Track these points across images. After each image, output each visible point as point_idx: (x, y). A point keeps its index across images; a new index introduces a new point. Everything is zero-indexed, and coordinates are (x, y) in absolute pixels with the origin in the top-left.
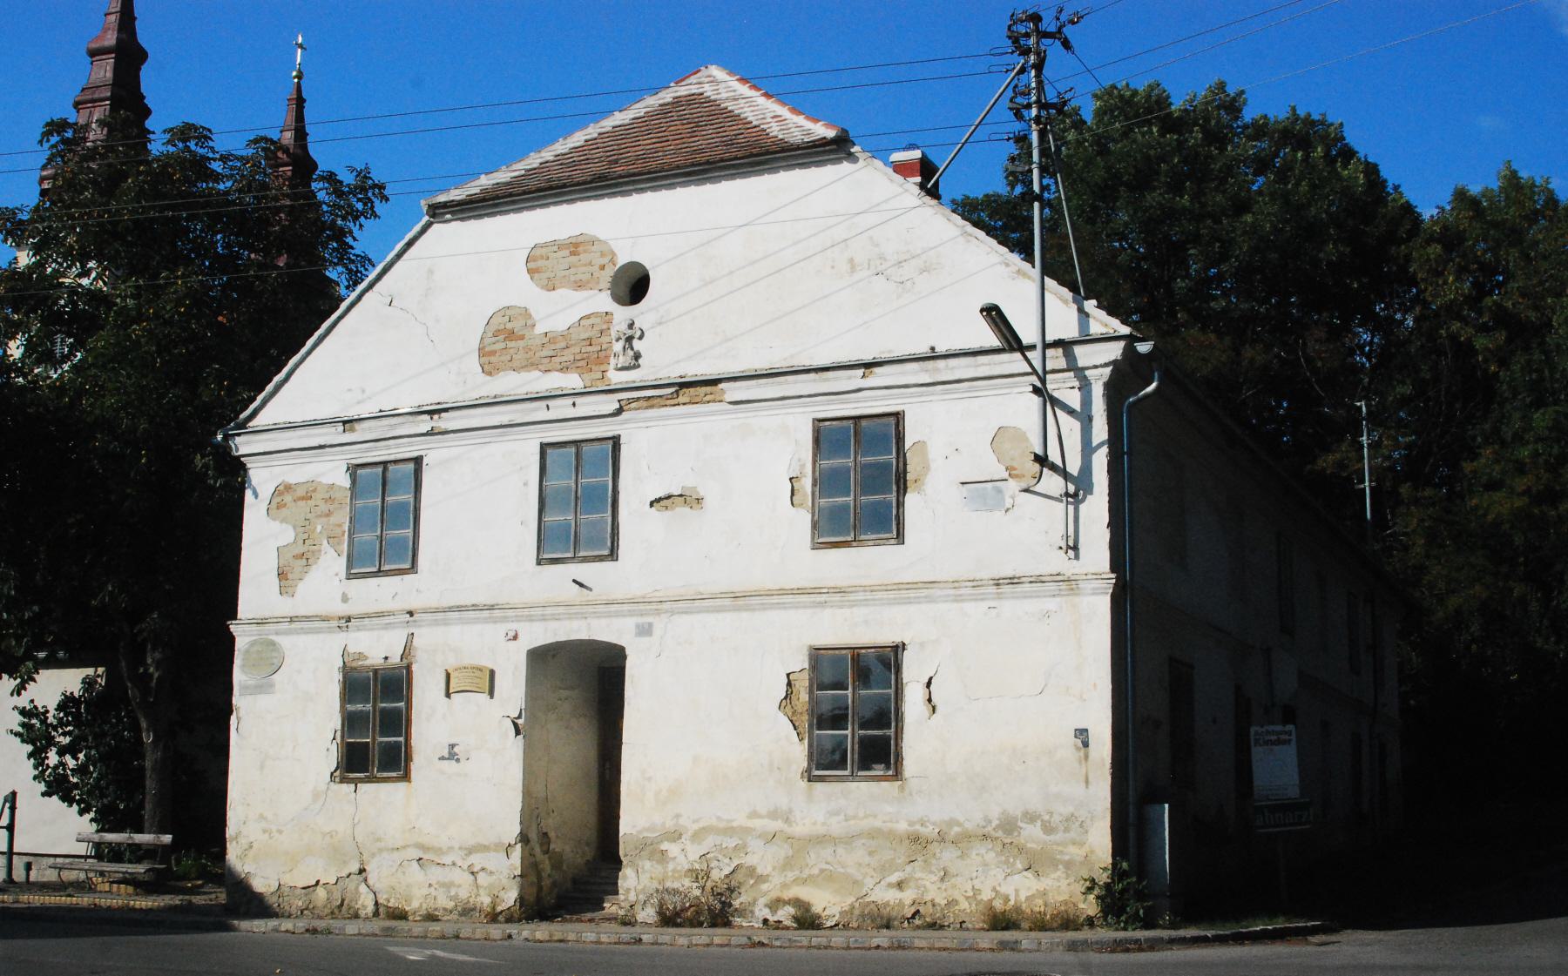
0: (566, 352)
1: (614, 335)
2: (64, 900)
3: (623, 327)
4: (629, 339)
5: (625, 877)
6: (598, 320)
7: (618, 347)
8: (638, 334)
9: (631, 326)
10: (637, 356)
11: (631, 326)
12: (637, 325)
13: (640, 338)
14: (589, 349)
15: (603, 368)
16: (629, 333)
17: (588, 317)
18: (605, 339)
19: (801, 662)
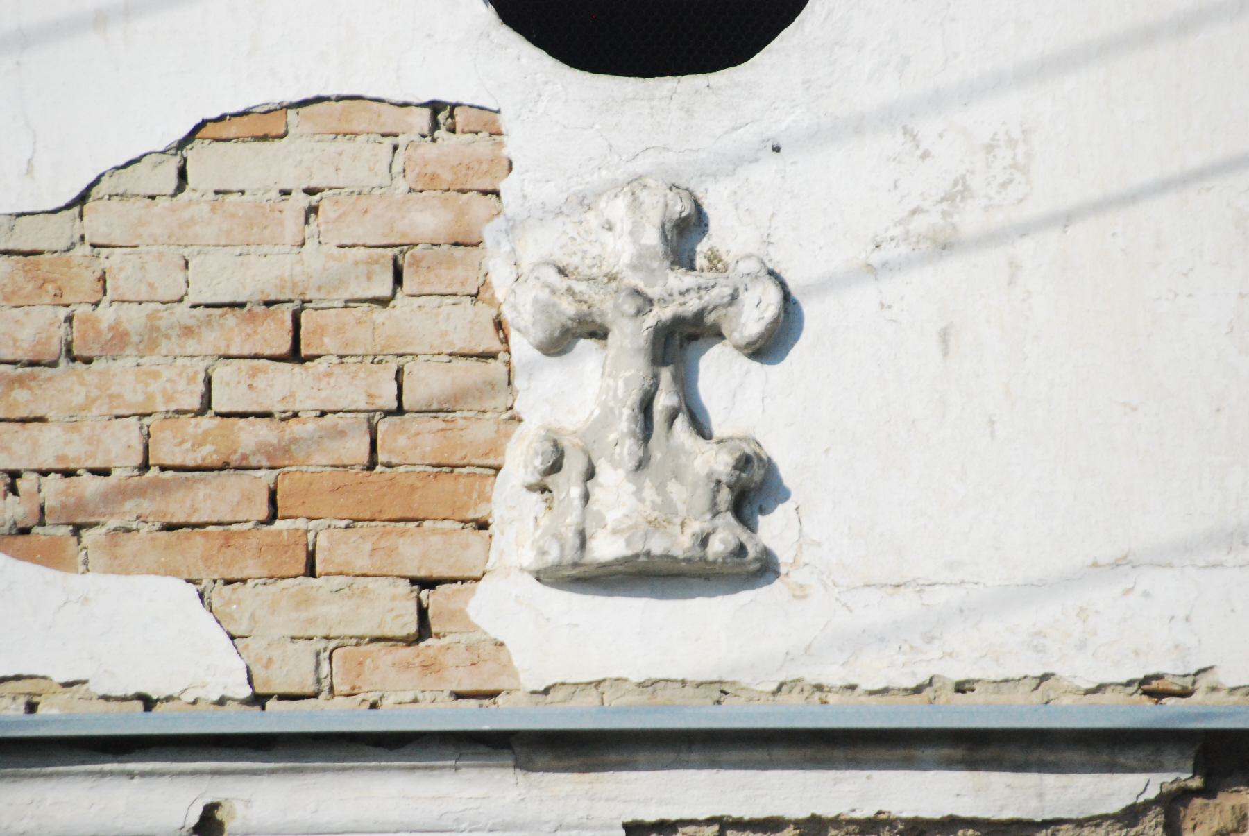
0: (66, 388)
1: (526, 306)
2: (432, 763)
3: (623, 240)
4: (679, 341)
5: (727, 464)
6: (361, 163)
7: (586, 393)
8: (757, 311)
9: (685, 234)
10: (751, 488)
11: (685, 234)
12: (727, 235)
13: (770, 346)
14: (281, 387)
15: (421, 551)
16: (677, 292)
17: (261, 125)
18: (430, 323)
19: (559, 326)
